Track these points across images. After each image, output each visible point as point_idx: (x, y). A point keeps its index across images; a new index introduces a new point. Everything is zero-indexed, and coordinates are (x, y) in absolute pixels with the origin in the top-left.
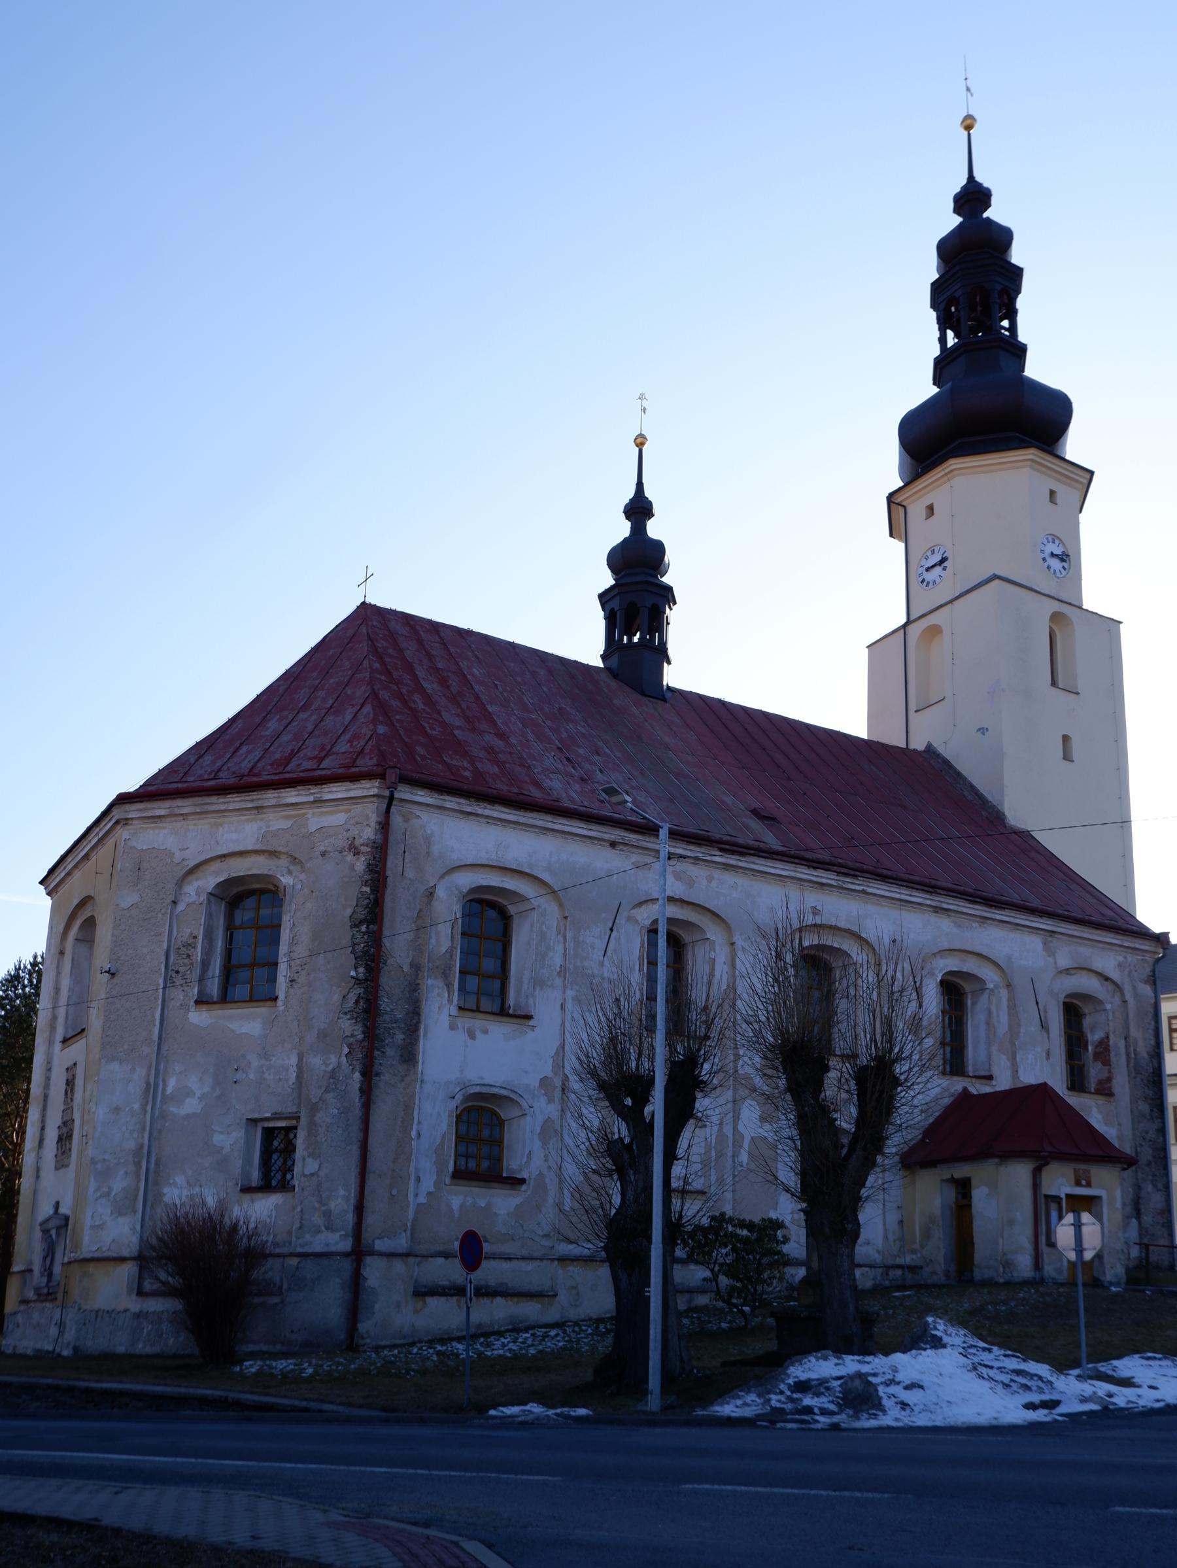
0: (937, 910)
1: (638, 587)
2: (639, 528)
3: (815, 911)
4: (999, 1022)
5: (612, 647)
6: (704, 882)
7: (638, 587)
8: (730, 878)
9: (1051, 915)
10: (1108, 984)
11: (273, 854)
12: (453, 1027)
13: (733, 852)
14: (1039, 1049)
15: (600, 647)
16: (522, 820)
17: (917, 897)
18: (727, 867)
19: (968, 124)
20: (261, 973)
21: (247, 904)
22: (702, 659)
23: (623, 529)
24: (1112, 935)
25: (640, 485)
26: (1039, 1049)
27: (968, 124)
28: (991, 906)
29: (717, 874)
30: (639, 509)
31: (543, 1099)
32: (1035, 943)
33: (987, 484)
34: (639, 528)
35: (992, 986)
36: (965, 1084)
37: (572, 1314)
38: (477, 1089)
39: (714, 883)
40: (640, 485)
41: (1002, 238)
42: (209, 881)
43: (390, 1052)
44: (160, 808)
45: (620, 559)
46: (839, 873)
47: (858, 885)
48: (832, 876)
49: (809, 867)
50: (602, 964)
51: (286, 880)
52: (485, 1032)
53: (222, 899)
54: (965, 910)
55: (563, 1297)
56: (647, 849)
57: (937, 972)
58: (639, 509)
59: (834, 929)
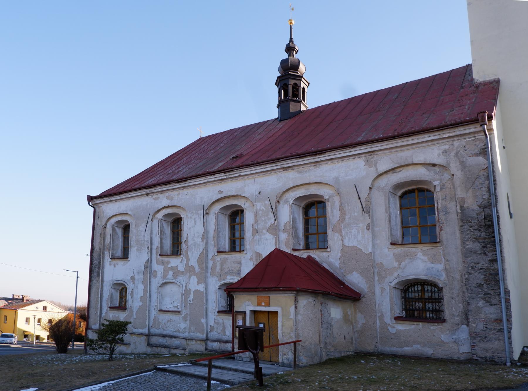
0: (284, 169)
3: (220, 192)
4: (333, 216)
6: (177, 197)
8: (186, 191)
9: (393, 138)
10: (437, 169)
12: (110, 265)
13: (181, 182)
14: (361, 225)
16: (121, 197)
17: (269, 167)
20: (321, 220)
24: (427, 135)
25: (291, 39)
26: (361, 225)
28: (316, 155)
29: (181, 192)
30: (290, 49)
31: (132, 283)
32: (360, 162)
35: (327, 197)
36: (308, 254)
37: (135, 351)
38: (115, 282)
39: (180, 196)
40: (291, 39)
43: (95, 274)
46: (225, 173)
47: (236, 173)
48: (223, 175)
49: (211, 175)
50: (144, 236)
52: (118, 264)
54: (299, 163)
55: (132, 346)
56: (156, 192)
57: (290, 200)
58: (290, 49)
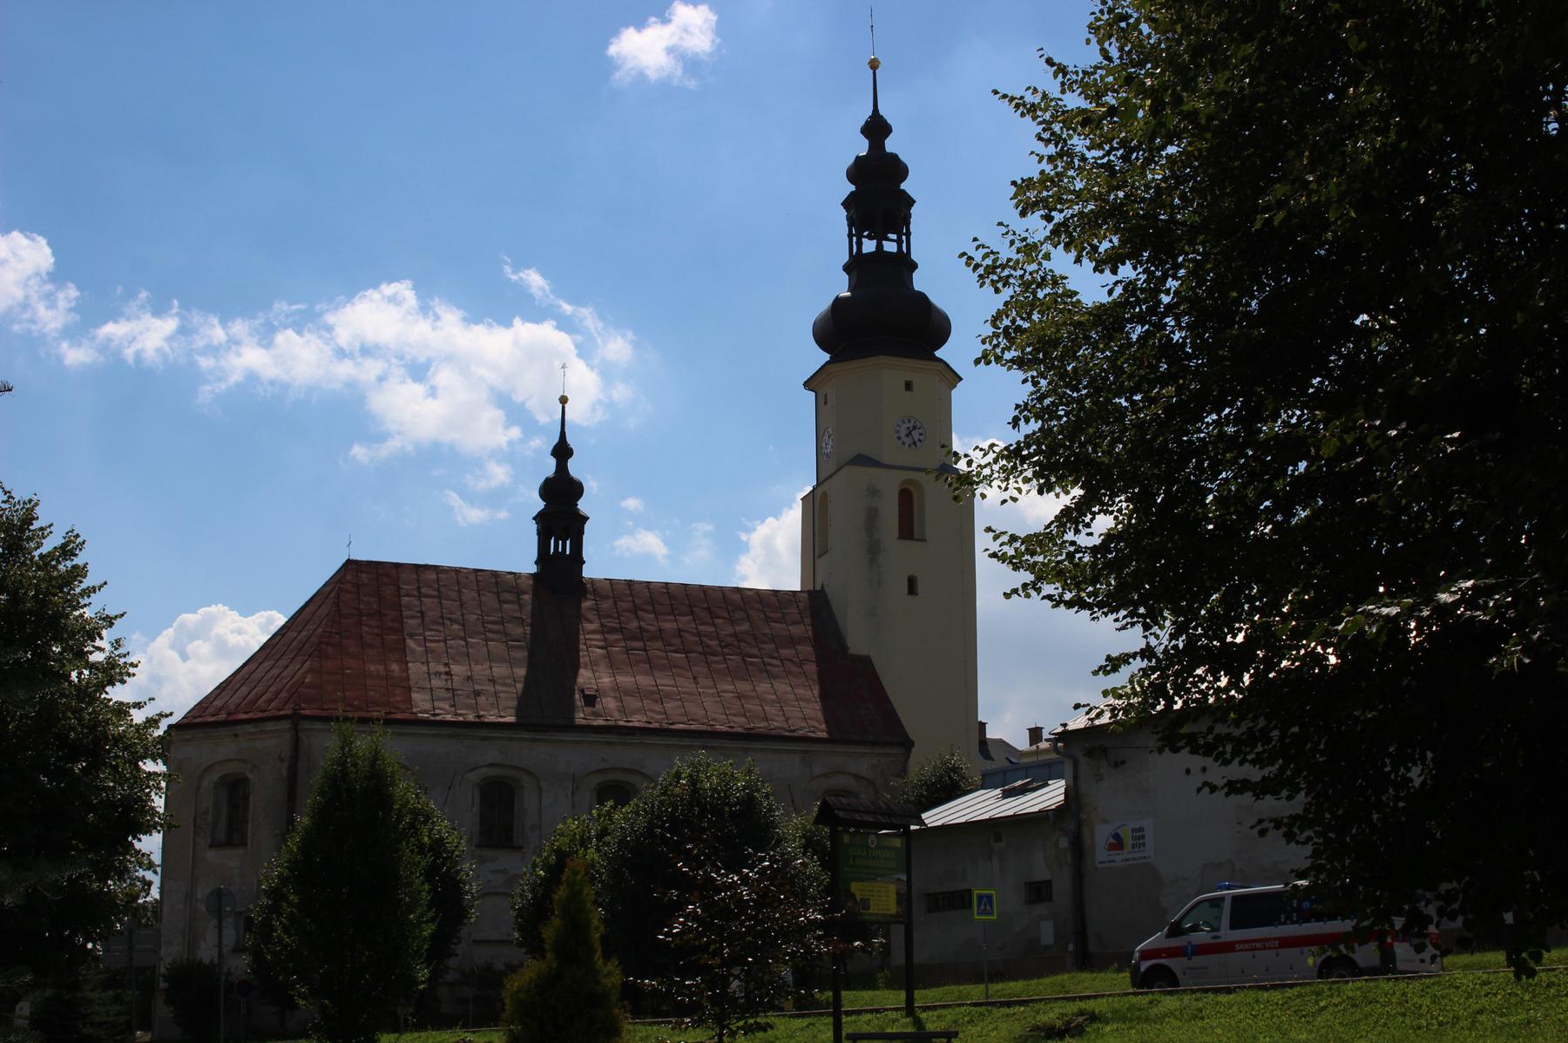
1: (561, 506)
2: (562, 467)
5: (543, 557)
7: (561, 506)
11: (244, 761)
15: (534, 555)
18: (535, 740)
19: (874, 65)
21: (235, 789)
22: (620, 549)
23: (549, 466)
27: (874, 65)
33: (887, 374)
34: (562, 467)
41: (898, 170)
42: (215, 776)
44: (188, 735)
45: (547, 489)
51: (251, 776)
53: (1032, 110)
59: (614, 769)
